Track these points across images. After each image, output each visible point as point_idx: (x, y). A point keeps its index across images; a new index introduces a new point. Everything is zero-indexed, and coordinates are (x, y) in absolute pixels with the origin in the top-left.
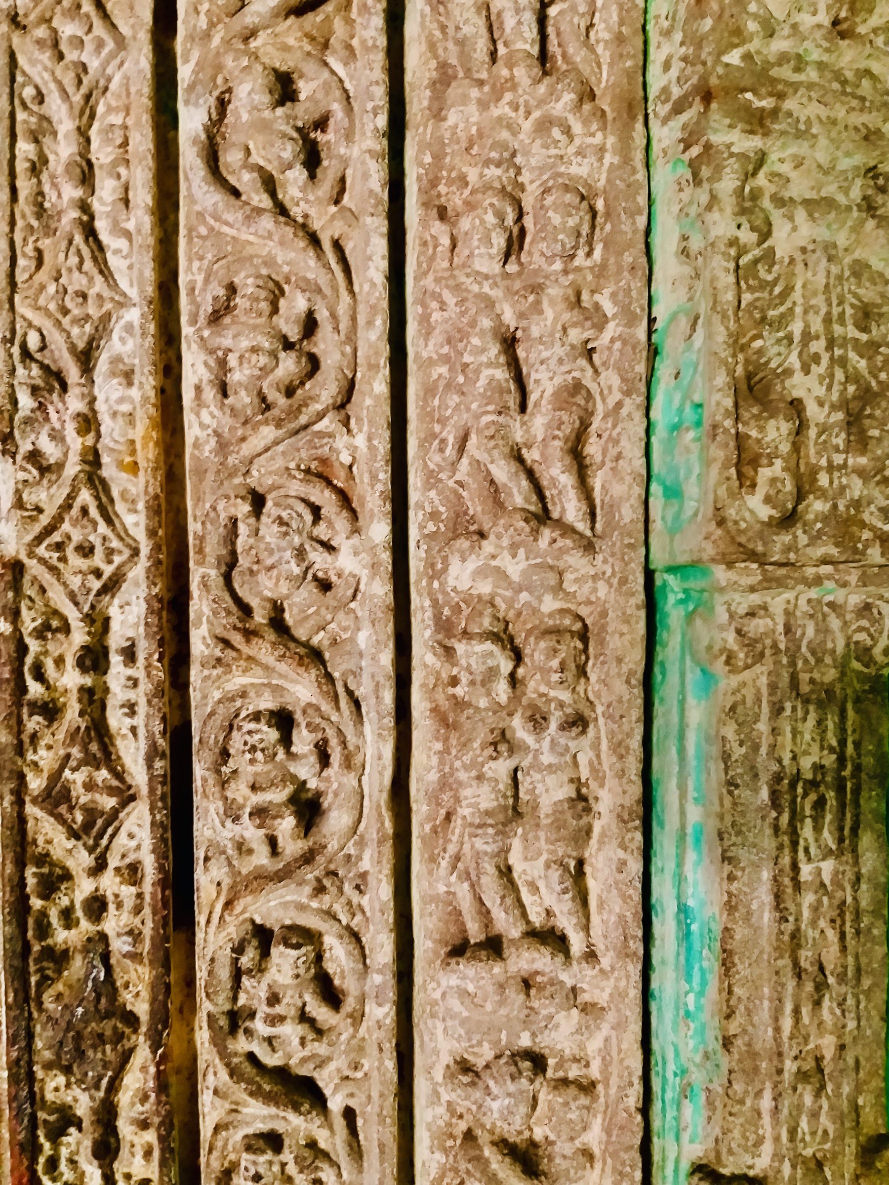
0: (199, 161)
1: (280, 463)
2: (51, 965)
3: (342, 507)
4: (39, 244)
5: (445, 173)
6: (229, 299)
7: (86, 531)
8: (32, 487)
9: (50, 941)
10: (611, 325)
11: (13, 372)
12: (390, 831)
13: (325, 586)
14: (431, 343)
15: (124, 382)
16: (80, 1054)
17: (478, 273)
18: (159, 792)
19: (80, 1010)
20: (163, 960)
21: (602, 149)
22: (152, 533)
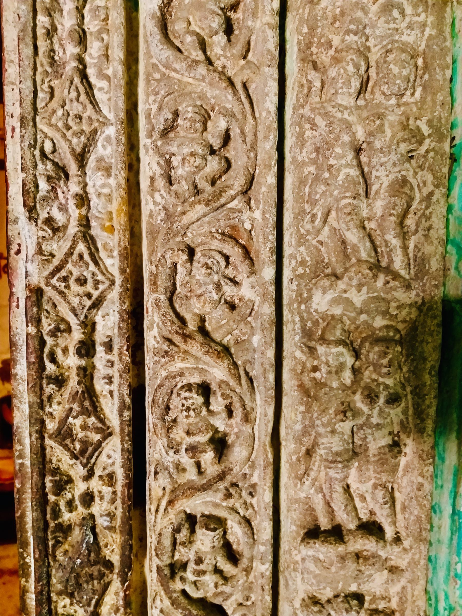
0: (156, 29)
1: (206, 229)
2: (61, 535)
3: (245, 257)
4: (52, 83)
5: (316, 40)
6: (174, 121)
7: (82, 269)
8: (48, 240)
9: (60, 520)
10: (427, 141)
11: (35, 166)
12: (271, 460)
13: (232, 307)
14: (304, 151)
15: (105, 174)
16: (79, 586)
17: (340, 105)
18: (126, 431)
19: (79, 561)
20: (128, 531)
21: (424, 25)
22: (123, 271)
